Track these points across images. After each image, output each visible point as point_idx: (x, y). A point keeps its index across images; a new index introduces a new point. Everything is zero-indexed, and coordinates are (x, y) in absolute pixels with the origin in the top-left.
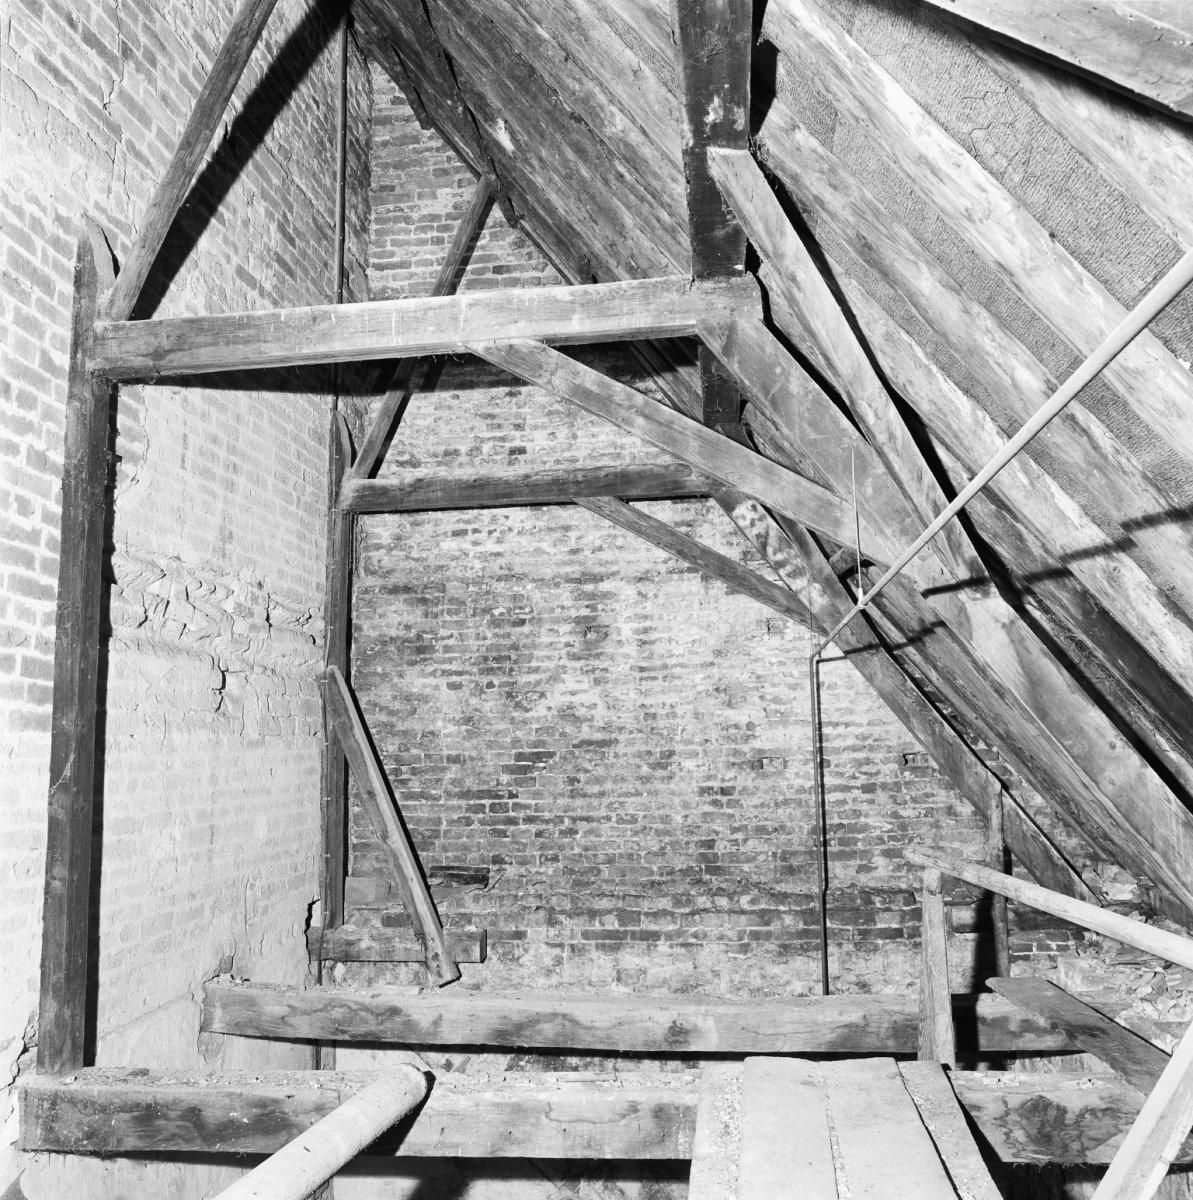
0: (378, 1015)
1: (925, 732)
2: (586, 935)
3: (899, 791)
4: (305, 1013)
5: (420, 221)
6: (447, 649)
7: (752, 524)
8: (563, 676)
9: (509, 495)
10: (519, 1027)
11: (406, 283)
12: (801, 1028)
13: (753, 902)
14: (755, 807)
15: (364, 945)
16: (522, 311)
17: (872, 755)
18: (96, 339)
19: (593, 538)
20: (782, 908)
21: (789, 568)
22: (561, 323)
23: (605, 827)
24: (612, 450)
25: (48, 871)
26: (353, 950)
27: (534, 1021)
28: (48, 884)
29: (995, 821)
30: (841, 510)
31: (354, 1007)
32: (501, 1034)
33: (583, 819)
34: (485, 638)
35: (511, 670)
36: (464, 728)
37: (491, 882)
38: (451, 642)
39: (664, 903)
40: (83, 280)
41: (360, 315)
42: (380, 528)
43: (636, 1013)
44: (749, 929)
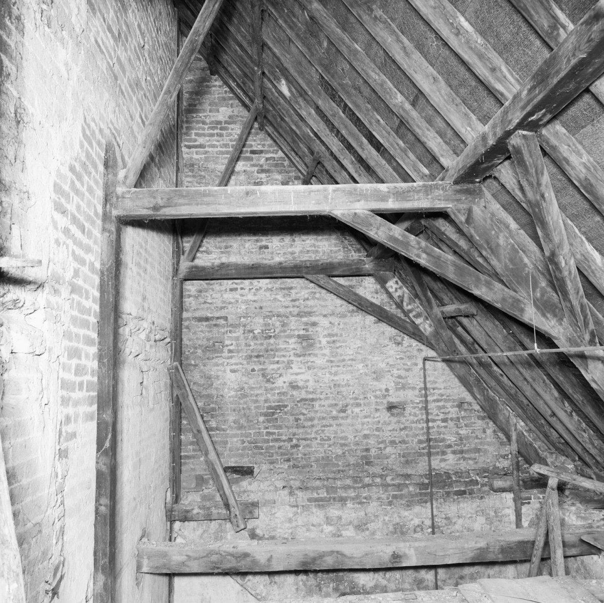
0: (236, 558)
1: (480, 394)
2: (310, 500)
3: (459, 421)
4: (195, 559)
5: (210, 124)
6: (230, 351)
7: (396, 290)
8: (292, 365)
9: (271, 273)
10: (314, 560)
11: (203, 156)
12: (457, 551)
13: (393, 479)
14: (390, 431)
15: (195, 512)
16: (363, 196)
17: (446, 404)
18: (118, 198)
19: (304, 293)
20: (407, 482)
21: (414, 313)
22: (383, 203)
23: (315, 443)
24: (313, 249)
25: (97, 501)
26: (189, 515)
27: (322, 556)
28: (97, 509)
29: (514, 438)
30: (525, 304)
31: (224, 554)
32: (304, 563)
33: (302, 439)
34: (250, 346)
35: (264, 362)
36: (239, 393)
37: (255, 474)
38: (231, 348)
39: (348, 482)
40: (109, 164)
41: (273, 193)
42: (192, 287)
43: (374, 549)
44: (392, 493)
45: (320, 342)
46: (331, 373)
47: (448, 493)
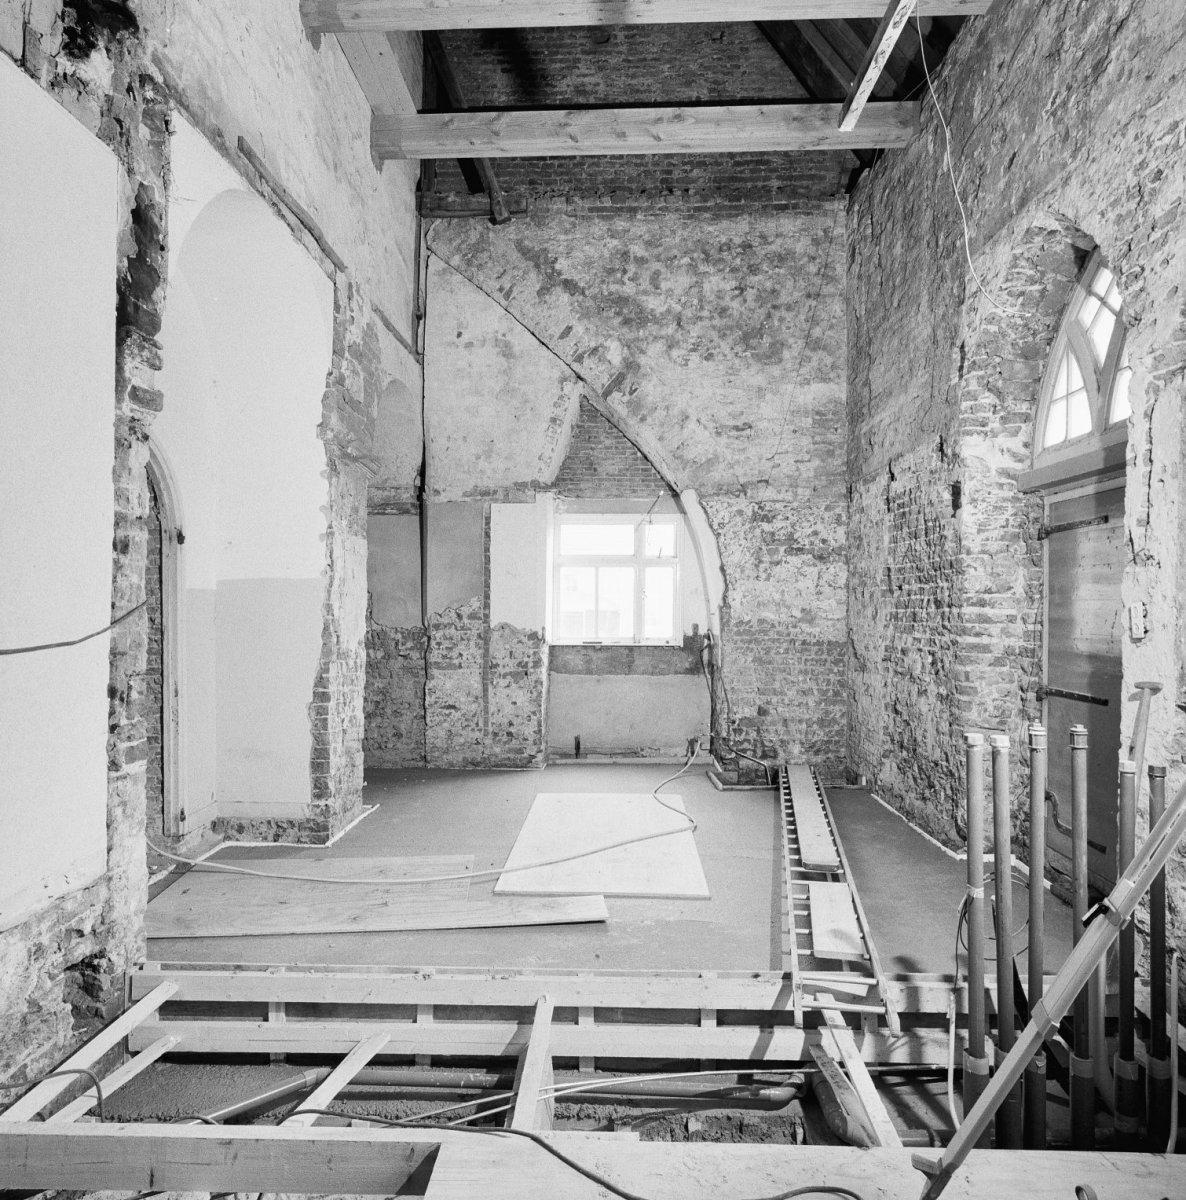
2: (591, 210)
45: (616, 37)
46: (627, 76)
47: (765, 207)
